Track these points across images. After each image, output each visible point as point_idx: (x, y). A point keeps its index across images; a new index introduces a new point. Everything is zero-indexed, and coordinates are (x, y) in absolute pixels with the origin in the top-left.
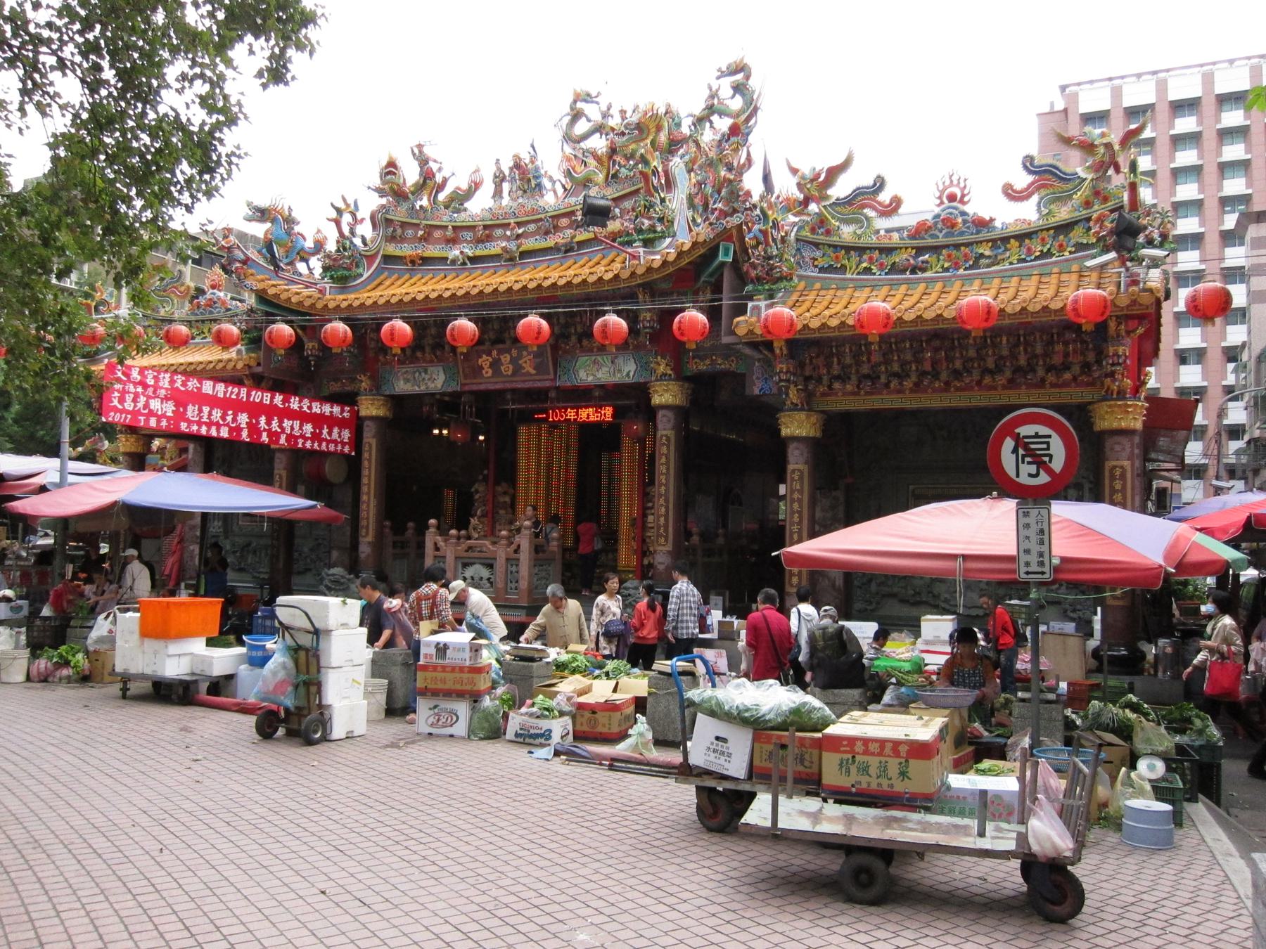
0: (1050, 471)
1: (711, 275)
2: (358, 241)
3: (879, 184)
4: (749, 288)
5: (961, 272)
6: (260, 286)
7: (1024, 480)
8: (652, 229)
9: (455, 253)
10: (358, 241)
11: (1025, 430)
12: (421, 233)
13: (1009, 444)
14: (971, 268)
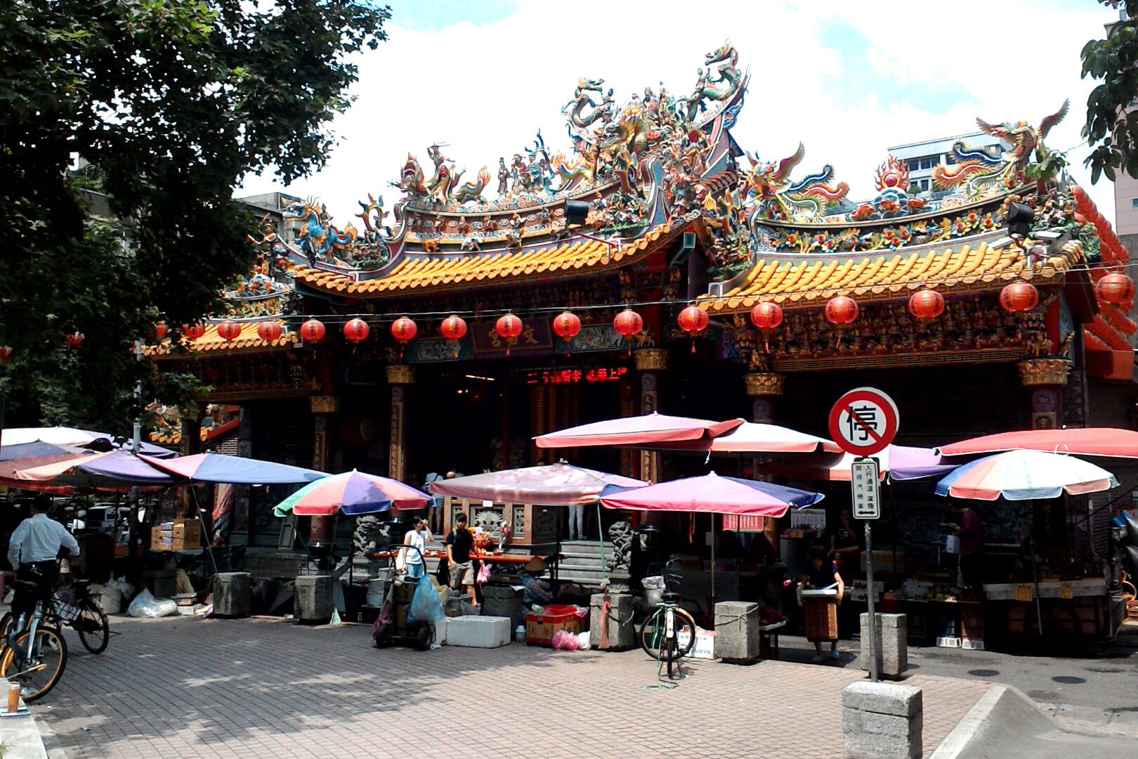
0: (875, 436)
1: (679, 259)
2: (383, 232)
3: (828, 173)
4: (711, 269)
5: (900, 248)
6: (300, 274)
7: (856, 442)
8: (629, 221)
9: (465, 240)
10: (383, 232)
11: (857, 405)
12: (438, 223)
13: (844, 415)
14: (909, 244)
